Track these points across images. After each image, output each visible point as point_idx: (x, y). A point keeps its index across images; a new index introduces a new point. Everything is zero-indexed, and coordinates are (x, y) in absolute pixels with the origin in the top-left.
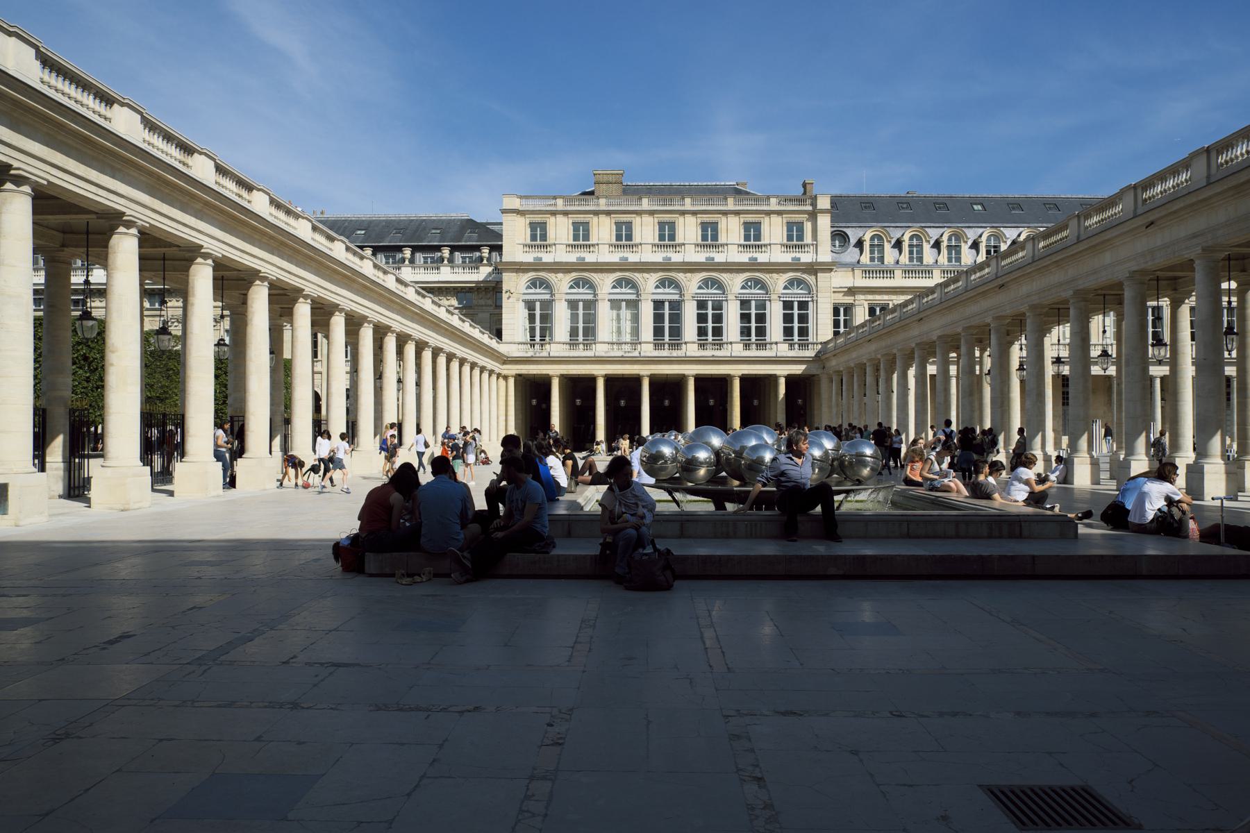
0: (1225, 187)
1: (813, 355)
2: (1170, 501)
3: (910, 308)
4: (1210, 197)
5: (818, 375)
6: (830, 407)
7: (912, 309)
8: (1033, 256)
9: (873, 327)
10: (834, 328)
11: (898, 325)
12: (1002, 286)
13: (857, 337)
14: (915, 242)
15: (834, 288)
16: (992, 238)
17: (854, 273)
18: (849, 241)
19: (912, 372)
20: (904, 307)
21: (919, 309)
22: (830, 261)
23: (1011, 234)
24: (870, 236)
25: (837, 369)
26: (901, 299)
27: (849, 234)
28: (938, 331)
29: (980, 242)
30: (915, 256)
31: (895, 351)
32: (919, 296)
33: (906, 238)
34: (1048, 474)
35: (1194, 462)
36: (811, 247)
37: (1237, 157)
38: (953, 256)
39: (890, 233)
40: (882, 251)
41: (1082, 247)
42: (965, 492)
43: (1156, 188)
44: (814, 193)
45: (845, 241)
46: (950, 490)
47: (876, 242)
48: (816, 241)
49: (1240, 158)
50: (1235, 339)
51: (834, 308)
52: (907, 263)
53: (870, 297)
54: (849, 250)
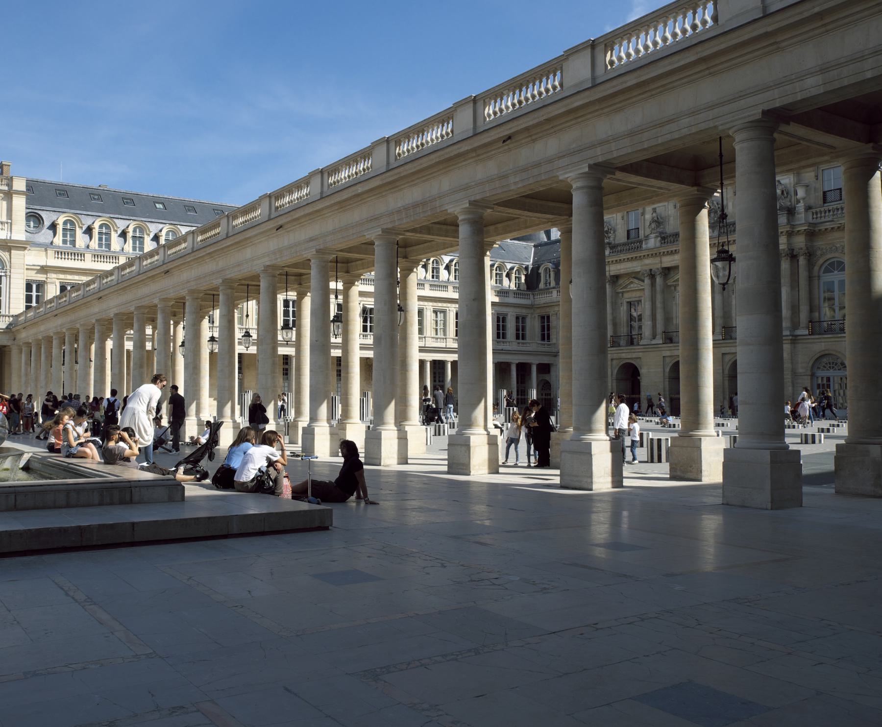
0: (333, 202)
1: (4, 327)
2: (271, 463)
3: (92, 287)
4: (323, 209)
5: (8, 346)
6: (20, 377)
7: (94, 288)
8: (193, 248)
9: (60, 303)
10: (26, 303)
11: (81, 302)
12: (167, 272)
13: (45, 312)
14: (104, 230)
15: (27, 265)
16: (171, 233)
17: (47, 253)
18: (43, 223)
19: (109, 344)
20: (87, 286)
21: (99, 288)
22: (24, 239)
23: (184, 230)
24: (63, 222)
25: (27, 341)
26: (85, 279)
27: (43, 217)
28: (115, 309)
29: (160, 236)
30: (104, 242)
31: (78, 326)
32: (100, 277)
33: (96, 226)
34: (200, 437)
35: (308, 425)
36: (6, 225)
37: (341, 179)
38: (138, 245)
39: (82, 220)
40: (73, 235)
41: (229, 242)
42: (98, 458)
43: (285, 198)
44: (11, 175)
45: (40, 223)
46: (83, 455)
47: (69, 227)
48: (11, 219)
49: (344, 181)
50: (340, 326)
51: (26, 284)
52: (97, 248)
53: (62, 276)
54: (43, 231)
